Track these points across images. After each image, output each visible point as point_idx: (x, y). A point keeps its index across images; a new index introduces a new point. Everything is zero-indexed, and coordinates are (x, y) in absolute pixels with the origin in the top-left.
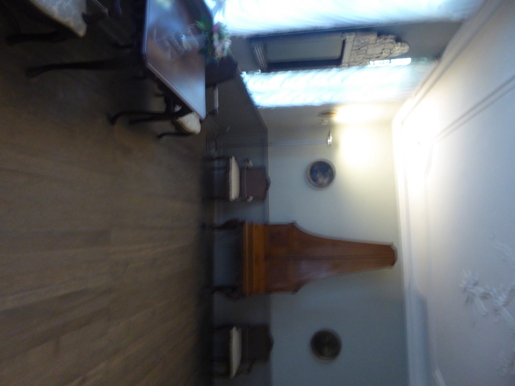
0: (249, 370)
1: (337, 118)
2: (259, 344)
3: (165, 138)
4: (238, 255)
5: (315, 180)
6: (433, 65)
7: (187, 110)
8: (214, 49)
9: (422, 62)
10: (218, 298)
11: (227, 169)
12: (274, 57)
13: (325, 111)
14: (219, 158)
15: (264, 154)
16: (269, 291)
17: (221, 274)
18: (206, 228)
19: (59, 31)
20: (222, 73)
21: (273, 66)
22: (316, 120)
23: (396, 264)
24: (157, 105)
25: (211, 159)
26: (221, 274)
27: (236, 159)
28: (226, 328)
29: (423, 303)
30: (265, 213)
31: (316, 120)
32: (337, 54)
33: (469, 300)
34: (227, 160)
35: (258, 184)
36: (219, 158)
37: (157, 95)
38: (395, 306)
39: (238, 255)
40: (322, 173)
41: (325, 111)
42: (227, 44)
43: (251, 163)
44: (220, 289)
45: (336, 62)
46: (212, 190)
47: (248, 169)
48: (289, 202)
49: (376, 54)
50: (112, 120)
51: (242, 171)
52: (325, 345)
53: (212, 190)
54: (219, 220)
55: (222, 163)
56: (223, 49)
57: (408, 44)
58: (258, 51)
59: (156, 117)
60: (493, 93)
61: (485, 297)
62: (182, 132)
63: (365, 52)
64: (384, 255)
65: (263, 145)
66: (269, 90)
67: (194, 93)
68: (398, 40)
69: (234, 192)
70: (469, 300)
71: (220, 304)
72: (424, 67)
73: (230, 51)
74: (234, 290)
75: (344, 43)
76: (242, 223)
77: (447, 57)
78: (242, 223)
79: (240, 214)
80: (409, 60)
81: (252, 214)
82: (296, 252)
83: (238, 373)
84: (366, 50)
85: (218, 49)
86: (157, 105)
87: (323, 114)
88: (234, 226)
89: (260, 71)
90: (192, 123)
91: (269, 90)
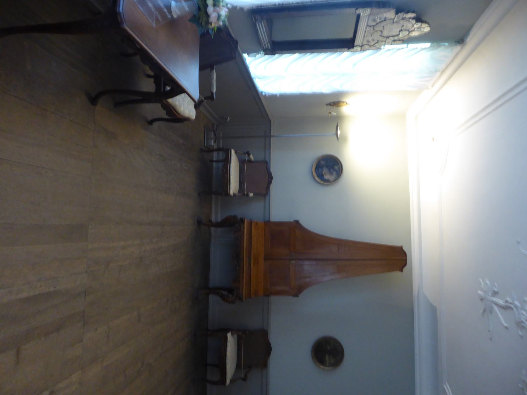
0: (245, 379)
1: (345, 109)
2: (257, 350)
3: (156, 124)
4: (236, 255)
5: (321, 176)
6: (458, 48)
7: (178, 89)
8: (208, 16)
9: (442, 48)
10: (213, 299)
11: (227, 161)
12: (279, 37)
13: (334, 101)
14: (218, 150)
15: (267, 147)
16: (268, 294)
17: (217, 276)
18: (202, 225)
19: (185, 120)
20: (219, 50)
21: (277, 47)
22: (324, 110)
23: (405, 269)
24: (148, 86)
25: (210, 150)
26: (217, 276)
27: (236, 152)
28: (222, 332)
29: (433, 311)
30: (267, 209)
31: (324, 110)
32: (351, 36)
33: (488, 311)
34: (227, 153)
35: (260, 179)
36: (218, 150)
37: (149, 76)
38: (403, 312)
39: (236, 255)
40: (329, 168)
41: (334, 101)
42: (224, 12)
43: (251, 156)
44: (216, 291)
45: (348, 44)
46: (210, 184)
47: (250, 161)
48: (294, 198)
49: (393, 36)
50: (93, 100)
51: (242, 163)
52: (327, 352)
53: (210, 184)
54: (217, 216)
55: (222, 155)
56: (219, 16)
57: (430, 26)
58: (262, 28)
59: (147, 98)
60: (504, 95)
61: (506, 308)
62: (174, 117)
63: (380, 33)
64: (394, 258)
65: (267, 136)
66: (274, 74)
67: (188, 75)
68: (418, 19)
69: (234, 187)
70: (488, 311)
71: (216, 306)
72: (445, 52)
73: (226, 20)
74: (231, 292)
75: (358, 17)
76: (242, 221)
77: (471, 41)
78: (242, 221)
79: (239, 211)
80: (428, 45)
81: (253, 211)
82: (297, 253)
83: (232, 381)
84: (381, 31)
85: (213, 16)
86: (148, 86)
87: (330, 104)
88: (233, 223)
89: (262, 53)
90: (185, 106)
91: (274, 74)
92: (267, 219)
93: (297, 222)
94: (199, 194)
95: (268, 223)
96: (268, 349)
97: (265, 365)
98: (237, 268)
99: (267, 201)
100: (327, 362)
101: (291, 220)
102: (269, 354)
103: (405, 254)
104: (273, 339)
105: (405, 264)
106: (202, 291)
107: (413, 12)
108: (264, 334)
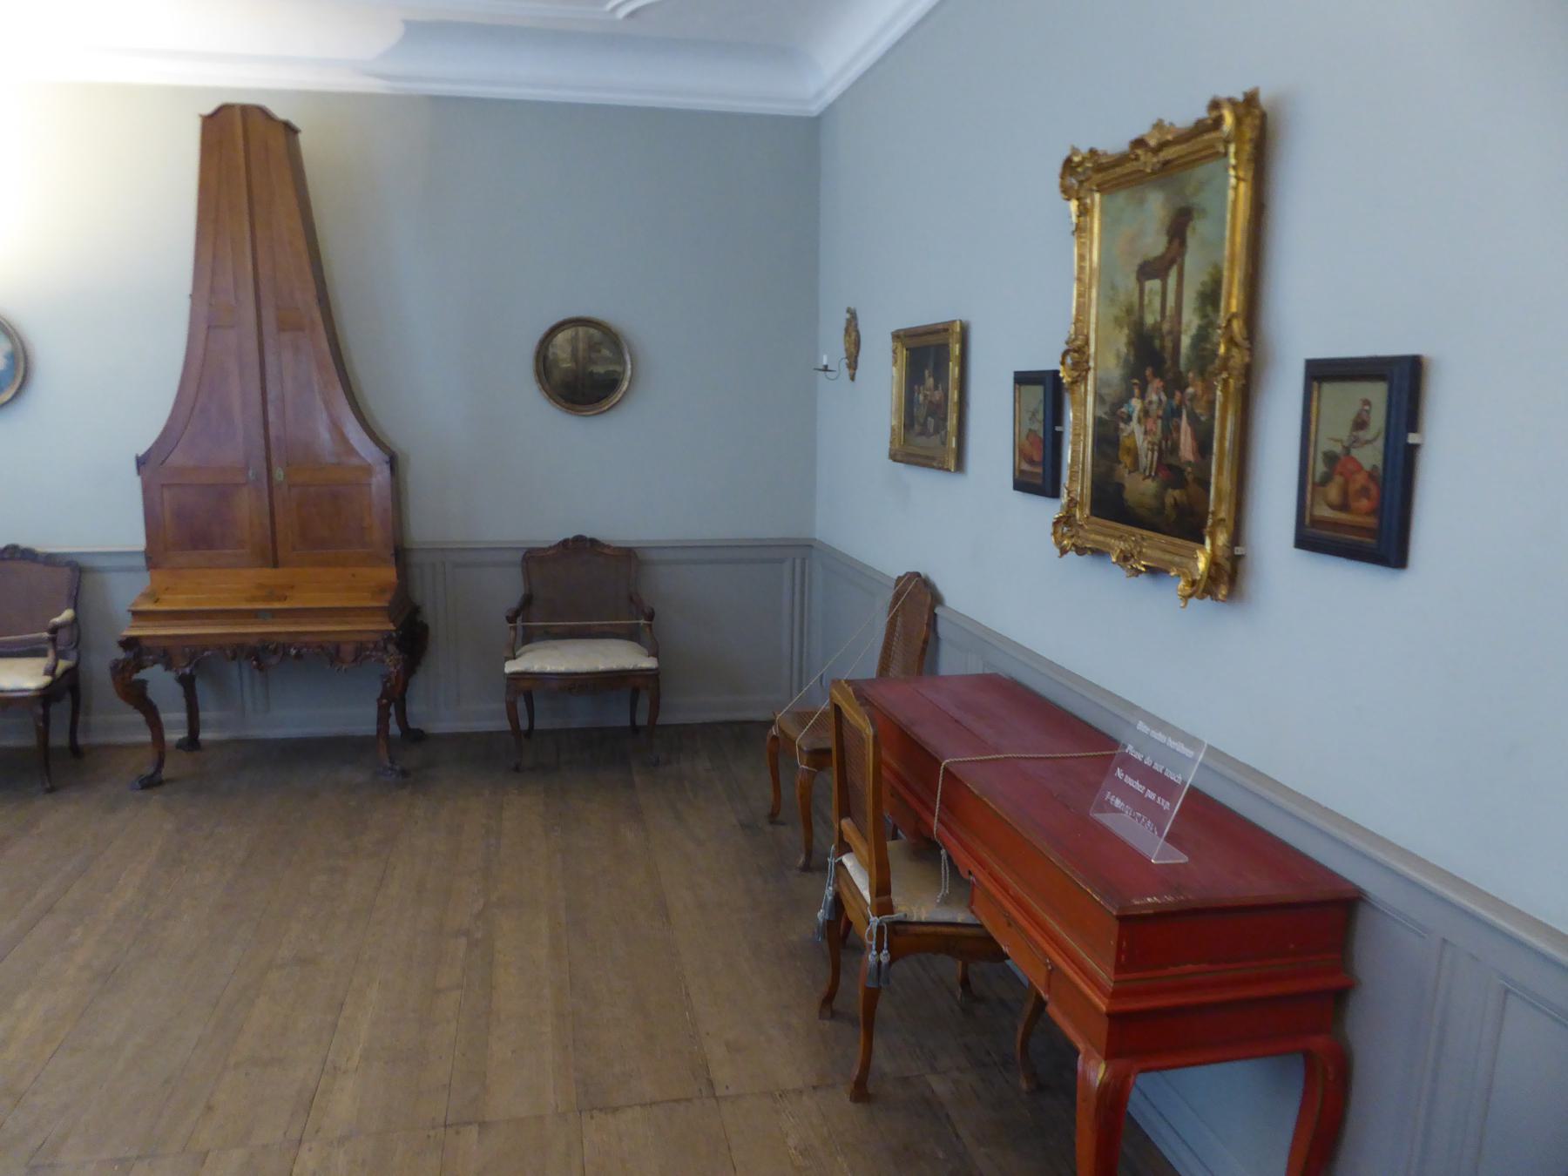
2: (582, 580)
16: (401, 555)
17: (352, 712)
71: (454, 703)
92: (141, 561)
93: (141, 462)
94: (51, 790)
95: (154, 557)
96: (580, 548)
97: (628, 558)
98: (293, 652)
99: (105, 563)
100: (611, 368)
101: (134, 484)
102: (594, 542)
103: (223, 111)
104: (550, 531)
105: (263, 112)
106: (403, 755)
107: (654, 653)
108: (534, 559)
